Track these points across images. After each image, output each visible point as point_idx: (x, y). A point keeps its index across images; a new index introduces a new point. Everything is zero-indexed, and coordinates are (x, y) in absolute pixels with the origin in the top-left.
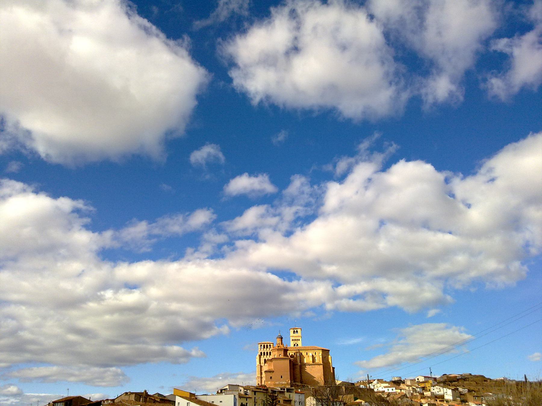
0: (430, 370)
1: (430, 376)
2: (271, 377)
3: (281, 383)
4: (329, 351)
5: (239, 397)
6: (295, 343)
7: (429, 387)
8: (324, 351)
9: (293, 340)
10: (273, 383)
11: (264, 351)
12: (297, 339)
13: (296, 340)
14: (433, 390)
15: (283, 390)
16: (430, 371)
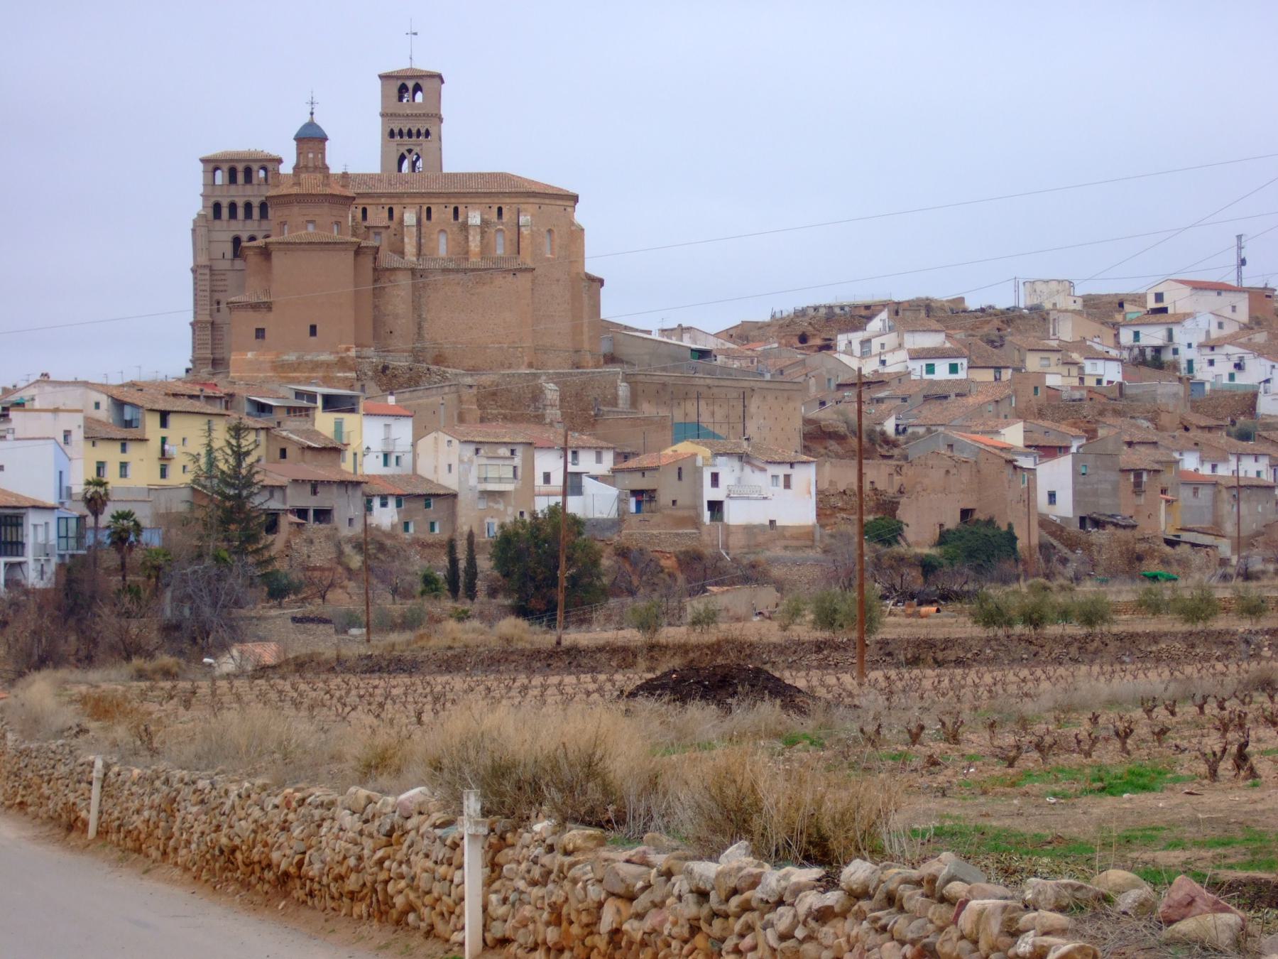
0: (1240, 248)
1: (1234, 283)
2: (258, 330)
3: (308, 358)
4: (575, 199)
5: (86, 438)
6: (403, 150)
7: (1190, 346)
8: (547, 201)
9: (396, 131)
10: (269, 357)
11: (229, 200)
12: (414, 131)
13: (410, 134)
14: (1205, 365)
15: (305, 403)
16: (1239, 254)
